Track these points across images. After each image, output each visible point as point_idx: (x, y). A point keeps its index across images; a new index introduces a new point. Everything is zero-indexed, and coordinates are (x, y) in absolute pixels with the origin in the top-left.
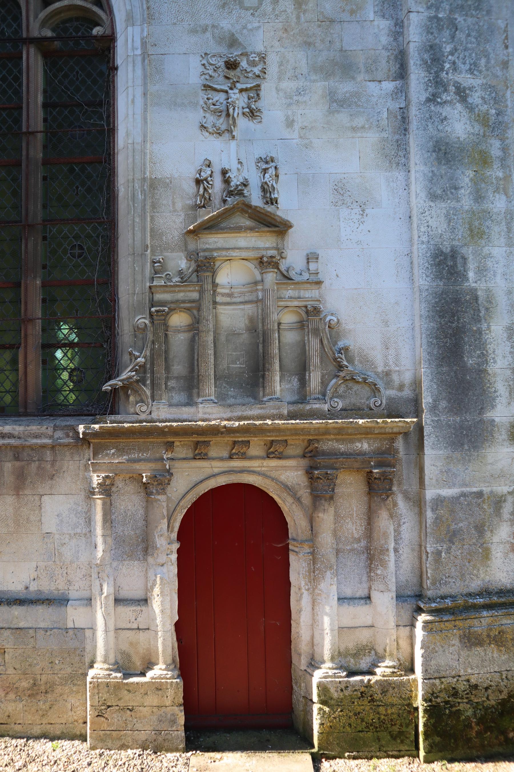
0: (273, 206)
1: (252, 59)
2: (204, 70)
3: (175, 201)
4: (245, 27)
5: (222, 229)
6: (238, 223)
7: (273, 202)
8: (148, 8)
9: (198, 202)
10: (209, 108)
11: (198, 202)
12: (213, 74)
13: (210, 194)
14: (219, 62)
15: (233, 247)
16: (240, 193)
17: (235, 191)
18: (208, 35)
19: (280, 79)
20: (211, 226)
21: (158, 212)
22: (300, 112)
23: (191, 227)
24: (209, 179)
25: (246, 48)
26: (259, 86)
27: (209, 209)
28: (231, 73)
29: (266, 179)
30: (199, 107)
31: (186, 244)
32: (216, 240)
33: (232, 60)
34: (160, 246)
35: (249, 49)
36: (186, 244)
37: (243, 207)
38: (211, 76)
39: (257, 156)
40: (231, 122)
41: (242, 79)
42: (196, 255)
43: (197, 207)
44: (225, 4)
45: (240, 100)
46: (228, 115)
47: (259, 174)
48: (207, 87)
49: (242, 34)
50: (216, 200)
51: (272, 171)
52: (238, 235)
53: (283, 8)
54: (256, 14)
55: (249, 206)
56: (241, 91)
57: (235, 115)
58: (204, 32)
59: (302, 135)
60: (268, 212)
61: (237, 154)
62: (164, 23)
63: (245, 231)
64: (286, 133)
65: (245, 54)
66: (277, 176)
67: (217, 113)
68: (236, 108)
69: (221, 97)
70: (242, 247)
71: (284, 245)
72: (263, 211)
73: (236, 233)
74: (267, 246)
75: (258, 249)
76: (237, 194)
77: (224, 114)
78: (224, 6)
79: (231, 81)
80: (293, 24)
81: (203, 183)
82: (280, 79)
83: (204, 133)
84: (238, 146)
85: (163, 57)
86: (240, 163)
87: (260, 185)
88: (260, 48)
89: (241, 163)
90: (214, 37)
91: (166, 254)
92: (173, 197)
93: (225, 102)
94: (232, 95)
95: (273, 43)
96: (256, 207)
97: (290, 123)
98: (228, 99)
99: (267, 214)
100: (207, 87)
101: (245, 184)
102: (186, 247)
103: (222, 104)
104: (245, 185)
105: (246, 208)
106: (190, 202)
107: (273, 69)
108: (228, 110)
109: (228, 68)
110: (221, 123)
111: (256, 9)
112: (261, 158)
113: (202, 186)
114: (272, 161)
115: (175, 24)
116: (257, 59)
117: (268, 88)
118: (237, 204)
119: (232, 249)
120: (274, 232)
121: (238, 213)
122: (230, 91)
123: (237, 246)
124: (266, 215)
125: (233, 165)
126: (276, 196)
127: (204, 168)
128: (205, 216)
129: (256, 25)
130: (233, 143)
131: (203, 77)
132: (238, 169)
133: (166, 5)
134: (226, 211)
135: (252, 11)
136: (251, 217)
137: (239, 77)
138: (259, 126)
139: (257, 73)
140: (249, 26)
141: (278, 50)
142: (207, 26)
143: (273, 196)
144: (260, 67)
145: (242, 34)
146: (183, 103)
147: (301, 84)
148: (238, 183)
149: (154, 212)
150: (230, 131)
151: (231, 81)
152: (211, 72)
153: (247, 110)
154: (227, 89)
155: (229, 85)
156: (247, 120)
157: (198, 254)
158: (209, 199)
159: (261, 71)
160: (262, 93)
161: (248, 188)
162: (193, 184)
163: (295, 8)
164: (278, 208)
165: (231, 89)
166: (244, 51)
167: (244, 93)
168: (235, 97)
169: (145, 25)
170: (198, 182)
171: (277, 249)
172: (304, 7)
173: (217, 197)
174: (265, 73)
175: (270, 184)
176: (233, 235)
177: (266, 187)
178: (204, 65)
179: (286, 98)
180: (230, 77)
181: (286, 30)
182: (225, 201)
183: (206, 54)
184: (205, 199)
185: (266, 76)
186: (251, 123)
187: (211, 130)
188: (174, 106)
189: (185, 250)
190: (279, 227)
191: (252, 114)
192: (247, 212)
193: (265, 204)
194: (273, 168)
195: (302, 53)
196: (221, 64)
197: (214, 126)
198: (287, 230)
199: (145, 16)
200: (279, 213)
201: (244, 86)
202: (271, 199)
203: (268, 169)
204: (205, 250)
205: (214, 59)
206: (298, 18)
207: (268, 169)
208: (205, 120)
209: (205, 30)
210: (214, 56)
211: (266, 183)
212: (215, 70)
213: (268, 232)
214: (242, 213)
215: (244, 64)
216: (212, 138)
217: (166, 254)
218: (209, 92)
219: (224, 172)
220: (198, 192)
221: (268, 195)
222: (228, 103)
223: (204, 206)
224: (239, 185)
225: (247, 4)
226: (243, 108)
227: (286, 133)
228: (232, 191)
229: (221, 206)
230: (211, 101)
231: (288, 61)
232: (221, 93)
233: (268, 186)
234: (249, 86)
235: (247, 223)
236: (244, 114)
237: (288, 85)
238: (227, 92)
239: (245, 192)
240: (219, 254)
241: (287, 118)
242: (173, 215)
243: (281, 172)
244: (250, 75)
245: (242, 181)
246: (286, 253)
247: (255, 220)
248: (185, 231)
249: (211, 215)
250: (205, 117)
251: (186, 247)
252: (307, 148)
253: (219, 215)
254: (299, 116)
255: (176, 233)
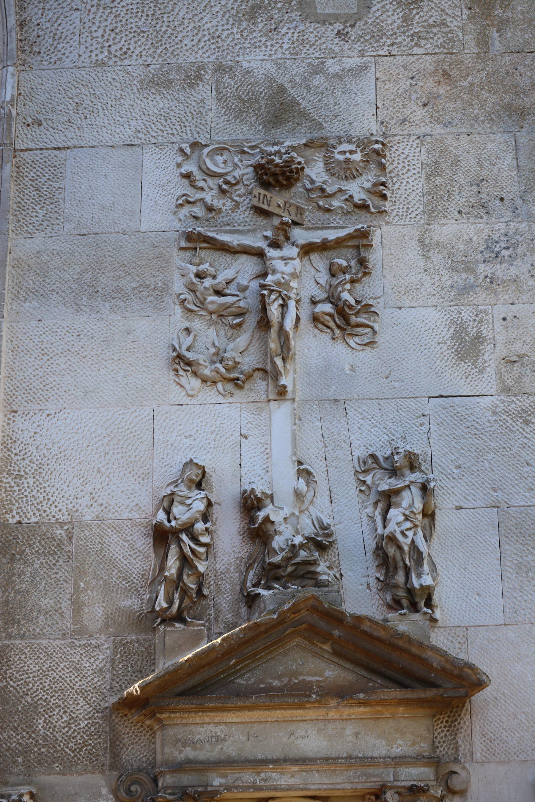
0: (417, 617)
1: (341, 158)
2: (189, 191)
3: (84, 598)
4: (317, 69)
5: (242, 694)
6: (295, 674)
7: (418, 600)
8: (21, 25)
9: (162, 603)
10: (202, 304)
11: (162, 603)
12: (217, 203)
13: (200, 575)
14: (236, 166)
15: (278, 754)
16: (305, 573)
17: (286, 566)
18: (205, 92)
19: (431, 213)
20: (202, 686)
21: (23, 637)
22: (500, 311)
23: (135, 688)
24: (200, 526)
25: (321, 127)
26: (364, 234)
27: (197, 626)
28: (276, 200)
29: (392, 527)
30: (169, 300)
31: (114, 747)
32: (219, 731)
33: (278, 160)
34: (26, 752)
35: (332, 130)
36: (114, 747)
37: (315, 619)
38: (210, 209)
39: (360, 452)
40: (273, 345)
41: (308, 217)
42: (149, 785)
43: (154, 619)
44: (255, 8)
45: (303, 279)
46: (264, 323)
47: (369, 510)
48: (196, 242)
49: (308, 88)
50: (223, 598)
51: (411, 500)
52: (297, 713)
53: (437, 17)
54: (353, 34)
55: (336, 617)
56: (308, 250)
57: (289, 325)
58: (191, 85)
59: (510, 382)
60: (402, 636)
61: (294, 445)
62: (67, 63)
63: (321, 702)
64: (457, 379)
65: (322, 145)
66: (429, 515)
67: (230, 318)
68: (292, 304)
69: (244, 269)
70: (311, 755)
71: (457, 749)
72: (382, 633)
73: (291, 707)
74: (397, 751)
75: (367, 761)
76: (292, 577)
77: (251, 320)
78: (252, 14)
79: (276, 222)
80: (468, 59)
81: (179, 541)
82: (431, 213)
83: (183, 381)
84: (297, 419)
85: (61, 154)
86: (304, 473)
87: (371, 544)
88: (366, 125)
89: (309, 473)
90: (221, 98)
91: (44, 779)
92: (76, 586)
93: (254, 285)
94: (279, 265)
95: (407, 112)
96: (359, 619)
97: (468, 347)
98: (264, 275)
99: (398, 644)
100: (196, 242)
101: (321, 542)
102: (115, 755)
103: (244, 289)
104: (322, 547)
105: (322, 624)
106: (131, 603)
107: (408, 185)
108: (264, 309)
109: (266, 185)
110: (243, 349)
111: (352, 20)
112: (373, 456)
113: (173, 550)
114: (413, 467)
115: (103, 64)
116: (357, 157)
117: (393, 245)
118: (294, 610)
119: (275, 761)
120: (421, 702)
121: (298, 640)
122: (272, 253)
123: (294, 753)
124: (395, 647)
125: (283, 482)
126: (427, 580)
127: (183, 490)
128: (180, 649)
129: (356, 61)
130: (281, 414)
131: (185, 211)
132: (298, 495)
133: (78, 14)
134: (257, 633)
135: (338, 26)
136: (340, 654)
137: (300, 211)
138: (366, 355)
139: (359, 196)
140: (333, 66)
141: (426, 130)
142: (201, 67)
143: (416, 582)
144: (367, 180)
145: (308, 88)
146: (119, 290)
147: (501, 227)
148: (298, 540)
149: (9, 636)
150: (270, 373)
151: (276, 222)
152: (209, 197)
153: (328, 308)
154: (262, 244)
155: (269, 233)
156: (326, 337)
157: (155, 781)
158: (199, 592)
159: (369, 191)
160: (374, 257)
161: (331, 555)
162: (144, 544)
163: (472, 17)
164: (434, 620)
165: (275, 245)
166: (317, 134)
167: (315, 257)
168: (288, 269)
169: (11, 69)
170: (162, 536)
171: (434, 761)
172: (498, 12)
173: (226, 586)
174: (384, 197)
175: (405, 542)
176: (278, 714)
177: (391, 551)
178: (188, 176)
179: (453, 269)
180: (270, 209)
181: (446, 74)
182: (251, 600)
183: (195, 145)
184: (185, 592)
185: (388, 206)
186: (340, 348)
187: (207, 372)
188: (91, 297)
189: (113, 767)
190: (442, 688)
191: (345, 319)
192: (326, 637)
193: (390, 607)
194: (415, 490)
195: (500, 138)
196: (244, 171)
197: (218, 356)
198: (468, 696)
199: (13, 45)
200: (439, 639)
201: (316, 237)
202: (410, 591)
203: (397, 492)
204: (180, 767)
205: (220, 159)
206: (483, 41)
207: (397, 492)
208: (188, 341)
209: (193, 78)
210: (221, 150)
211: (392, 538)
212: (223, 192)
213: (401, 702)
214: (309, 640)
215: (316, 171)
216: (210, 395)
217: (44, 779)
218: (203, 253)
219: (250, 504)
220: (162, 568)
221: (400, 578)
222: (263, 287)
223: (179, 618)
224: (302, 546)
225: (324, 7)
226: (314, 302)
227: (457, 379)
228: (276, 566)
229: (238, 614)
230: (208, 282)
231: (456, 162)
232: (244, 258)
233: (399, 547)
234: (332, 235)
235: (328, 673)
236: (315, 319)
237: (458, 231)
238: (260, 254)
239: (321, 568)
240: (230, 780)
241: (459, 330)
242: (72, 646)
243: (443, 502)
244: (336, 203)
245: (309, 530)
246: (463, 774)
247: (356, 662)
248: (114, 699)
249: (204, 646)
250: (188, 330)
251: (115, 755)
252: (527, 422)
253: (230, 649)
254: (499, 325)
255: (82, 708)
